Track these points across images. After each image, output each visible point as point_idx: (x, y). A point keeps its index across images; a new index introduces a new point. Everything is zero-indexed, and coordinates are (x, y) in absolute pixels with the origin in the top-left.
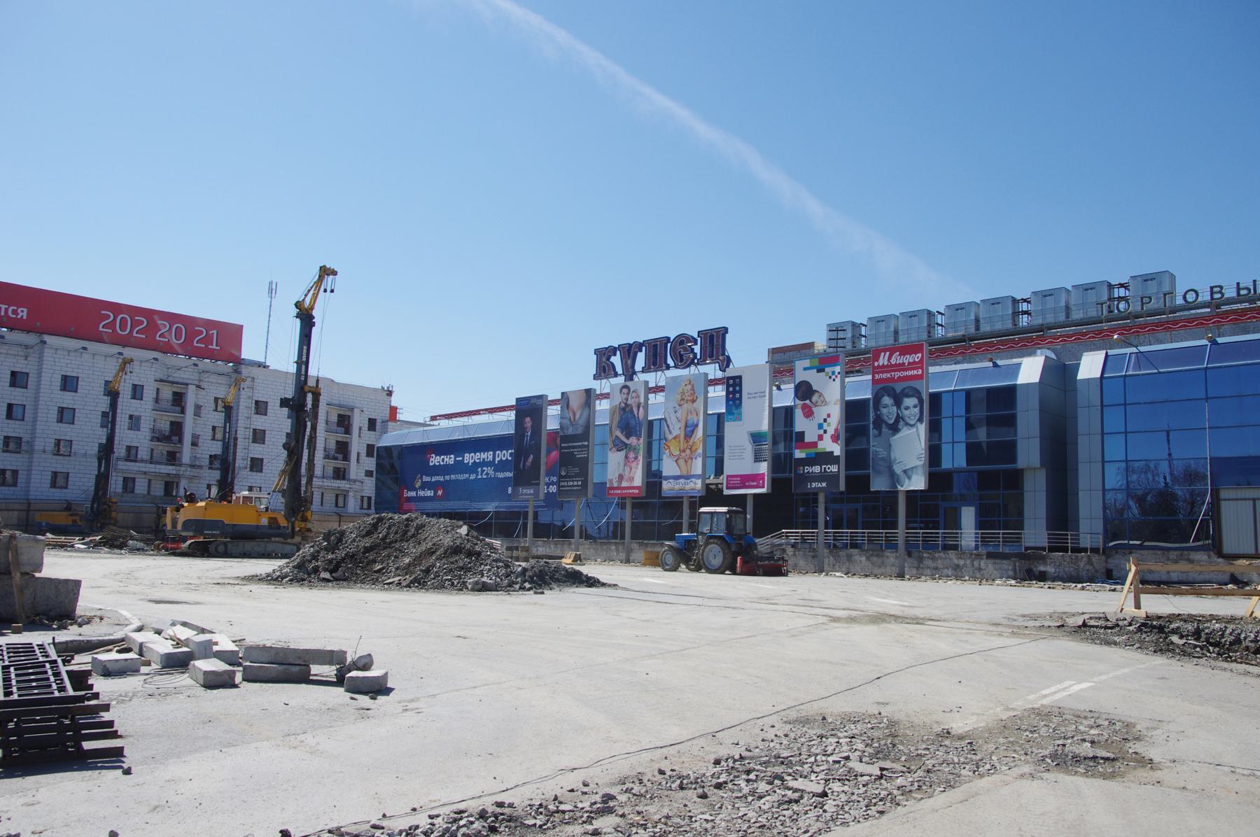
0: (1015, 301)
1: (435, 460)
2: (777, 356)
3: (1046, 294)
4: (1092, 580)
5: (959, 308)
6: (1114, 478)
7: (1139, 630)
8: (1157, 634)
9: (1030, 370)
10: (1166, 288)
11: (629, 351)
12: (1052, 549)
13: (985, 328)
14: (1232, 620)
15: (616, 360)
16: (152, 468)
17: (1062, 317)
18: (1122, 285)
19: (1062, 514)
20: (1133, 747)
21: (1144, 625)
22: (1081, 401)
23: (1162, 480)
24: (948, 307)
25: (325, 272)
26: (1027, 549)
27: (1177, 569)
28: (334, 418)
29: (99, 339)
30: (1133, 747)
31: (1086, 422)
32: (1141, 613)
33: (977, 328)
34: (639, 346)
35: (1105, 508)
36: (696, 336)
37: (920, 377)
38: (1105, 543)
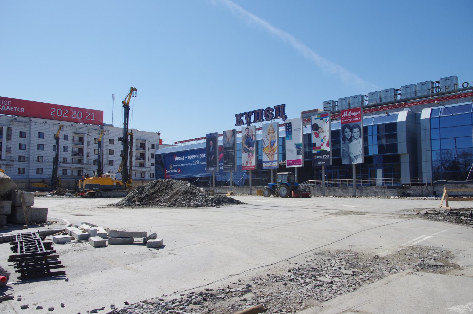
0: (395, 90)
1: (177, 159)
2: (304, 115)
3: (407, 87)
5: (373, 94)
7: (448, 214)
8: (455, 216)
10: (455, 83)
11: (248, 115)
12: (412, 185)
13: (384, 101)
15: (244, 118)
16: (72, 165)
17: (413, 96)
18: (437, 82)
19: (416, 171)
22: (422, 127)
23: (454, 156)
24: (369, 93)
25: (133, 89)
26: (402, 184)
28: (139, 144)
29: (51, 118)
31: (424, 136)
32: (449, 208)
33: (381, 101)
34: (252, 113)
36: (273, 108)
37: (360, 120)
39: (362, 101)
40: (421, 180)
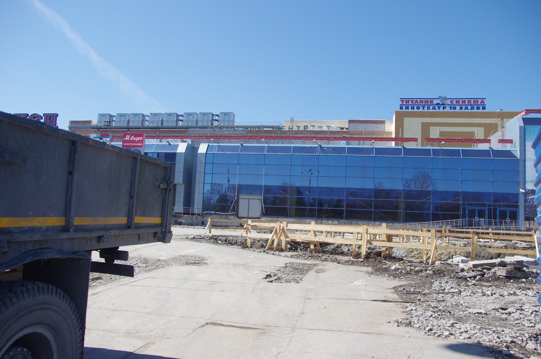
0: (178, 115)
2: (74, 125)
3: (190, 114)
4: (197, 225)
5: (155, 115)
6: (208, 187)
7: (210, 239)
8: (215, 239)
9: (182, 148)
10: (232, 119)
12: (184, 214)
13: (165, 124)
14: (236, 236)
18: (217, 115)
19: (188, 202)
20: (205, 261)
21: (211, 238)
22: (198, 161)
23: (224, 189)
24: (151, 114)
26: (176, 213)
27: (224, 221)
30: (203, 261)
31: (200, 169)
32: (211, 235)
33: (162, 124)
35: (203, 201)
36: (42, 115)
37: (142, 146)
38: (203, 211)
39: (143, 121)
40: (193, 210)
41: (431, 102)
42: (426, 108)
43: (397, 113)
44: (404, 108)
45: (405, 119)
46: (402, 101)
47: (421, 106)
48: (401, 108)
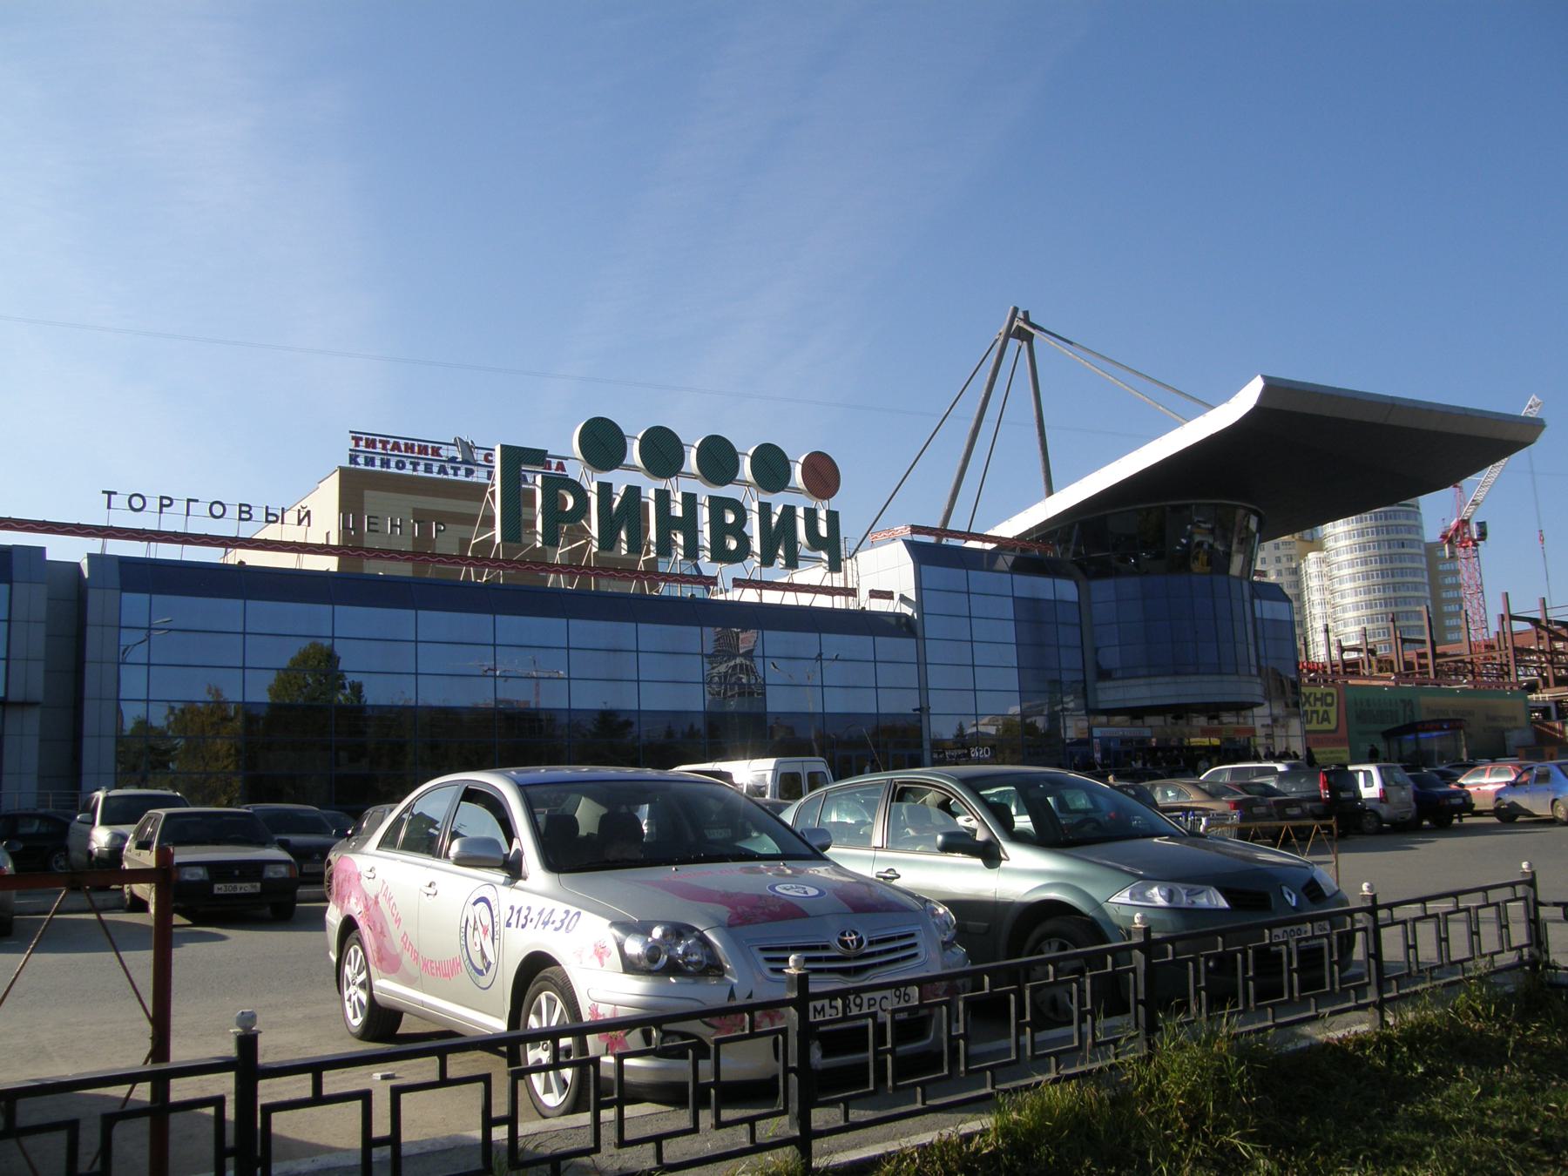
41: (436, 451)
42: (421, 468)
43: (344, 473)
44: (361, 460)
45: (367, 492)
46: (357, 440)
47: (407, 462)
48: (353, 459)
